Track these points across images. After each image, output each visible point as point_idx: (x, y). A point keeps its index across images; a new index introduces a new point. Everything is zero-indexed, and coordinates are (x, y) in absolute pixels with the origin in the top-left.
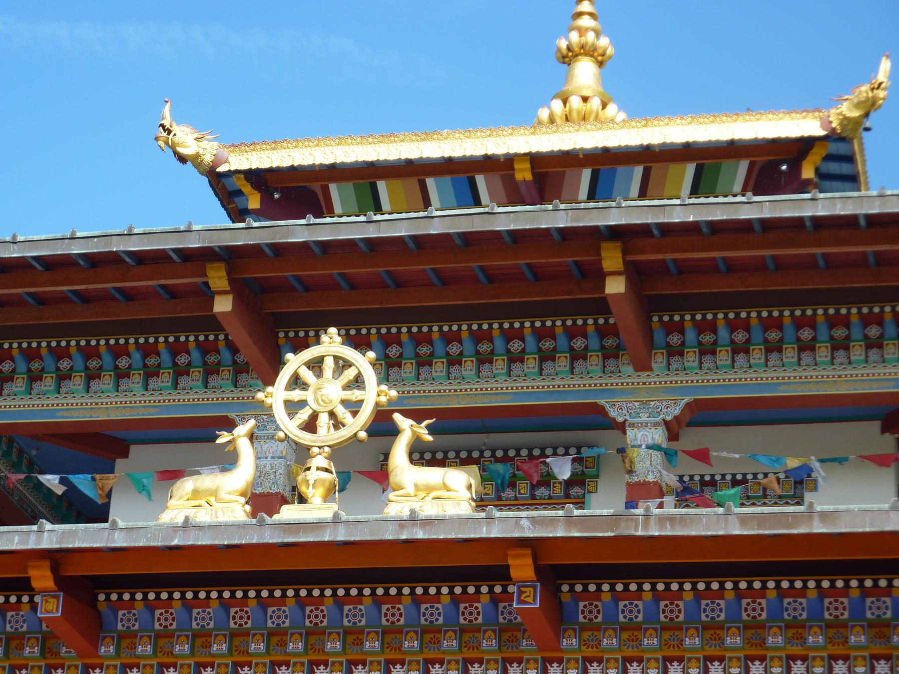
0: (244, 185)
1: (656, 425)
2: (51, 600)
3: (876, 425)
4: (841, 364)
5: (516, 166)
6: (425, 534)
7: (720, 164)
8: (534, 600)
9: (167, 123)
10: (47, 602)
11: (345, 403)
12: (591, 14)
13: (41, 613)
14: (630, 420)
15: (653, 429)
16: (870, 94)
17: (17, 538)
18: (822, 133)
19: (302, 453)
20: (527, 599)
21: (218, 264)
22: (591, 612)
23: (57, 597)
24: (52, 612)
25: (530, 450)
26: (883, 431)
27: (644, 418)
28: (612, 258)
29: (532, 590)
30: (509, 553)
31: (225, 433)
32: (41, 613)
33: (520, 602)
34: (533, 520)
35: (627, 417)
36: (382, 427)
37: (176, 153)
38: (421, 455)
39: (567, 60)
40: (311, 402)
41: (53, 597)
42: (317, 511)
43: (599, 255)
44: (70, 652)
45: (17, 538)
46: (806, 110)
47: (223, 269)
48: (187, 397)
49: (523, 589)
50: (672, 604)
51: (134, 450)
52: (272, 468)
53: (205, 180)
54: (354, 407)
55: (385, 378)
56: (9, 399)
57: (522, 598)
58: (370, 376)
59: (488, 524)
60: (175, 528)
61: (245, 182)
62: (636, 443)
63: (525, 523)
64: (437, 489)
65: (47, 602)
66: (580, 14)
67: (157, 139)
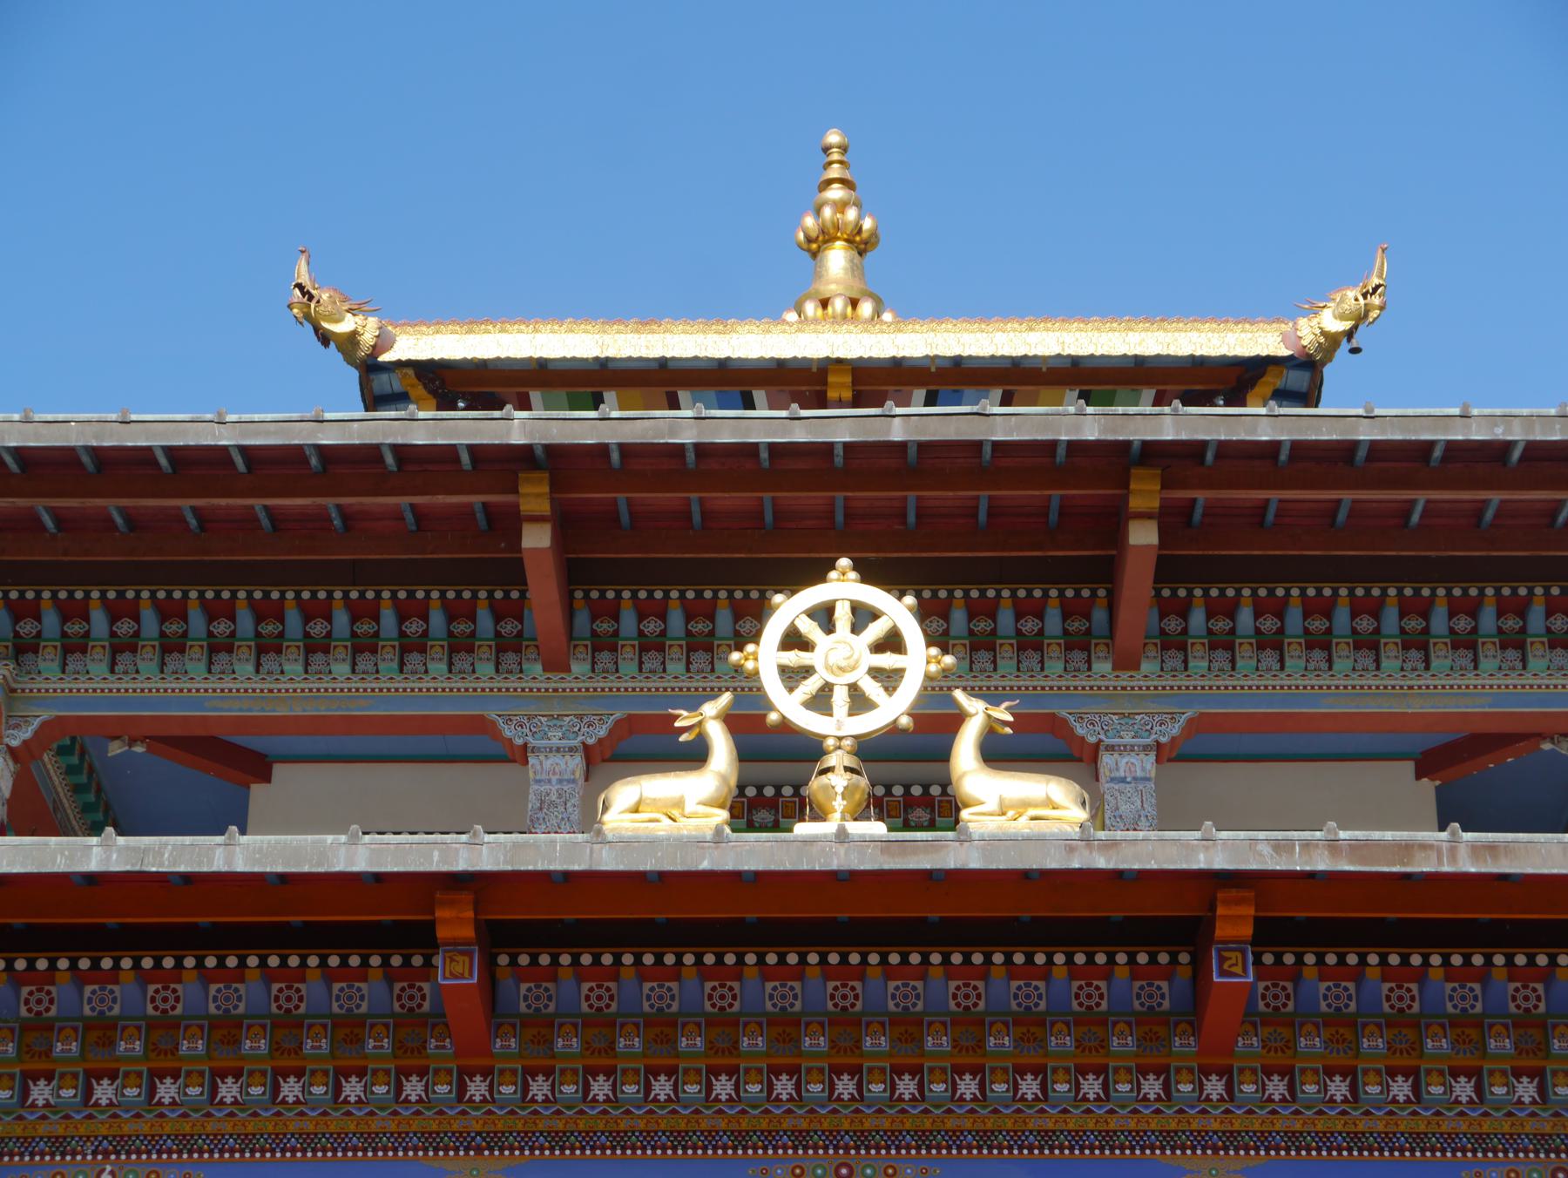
0: (413, 386)
1: (1146, 748)
2: (460, 958)
3: (1409, 766)
4: (1414, 669)
5: (831, 379)
6: (1108, 861)
7: (1114, 392)
8: (1245, 969)
9: (304, 279)
10: (452, 960)
11: (876, 673)
12: (842, 181)
13: (445, 978)
14: (1108, 741)
15: (1142, 755)
16: (1362, 301)
17: (436, 854)
18: (1285, 352)
19: (810, 750)
20: (1234, 969)
21: (536, 475)
22: (1276, 997)
23: (470, 954)
24: (462, 977)
25: (907, 788)
26: (1418, 777)
27: (1128, 739)
28: (1145, 493)
29: (1239, 955)
30: (1219, 895)
31: (685, 713)
32: (445, 978)
33: (1223, 973)
34: (1278, 847)
35: (1102, 737)
36: (936, 688)
37: (317, 329)
38: (995, 753)
39: (814, 246)
40: (819, 667)
41: (462, 953)
42: (839, 832)
43: (1127, 486)
44: (444, 1047)
45: (436, 854)
46: (1273, 317)
47: (546, 482)
48: (417, 685)
49: (1225, 954)
50: (1400, 987)
51: (278, 770)
52: (560, 796)
53: (354, 374)
54: (889, 679)
55: (938, 640)
56: (126, 678)
57: (1226, 967)
58: (913, 633)
59: (1207, 848)
60: (699, 842)
61: (416, 381)
62: (1117, 774)
63: (1265, 849)
64: (1036, 805)
65: (452, 960)
66: (830, 182)
67: (290, 307)
